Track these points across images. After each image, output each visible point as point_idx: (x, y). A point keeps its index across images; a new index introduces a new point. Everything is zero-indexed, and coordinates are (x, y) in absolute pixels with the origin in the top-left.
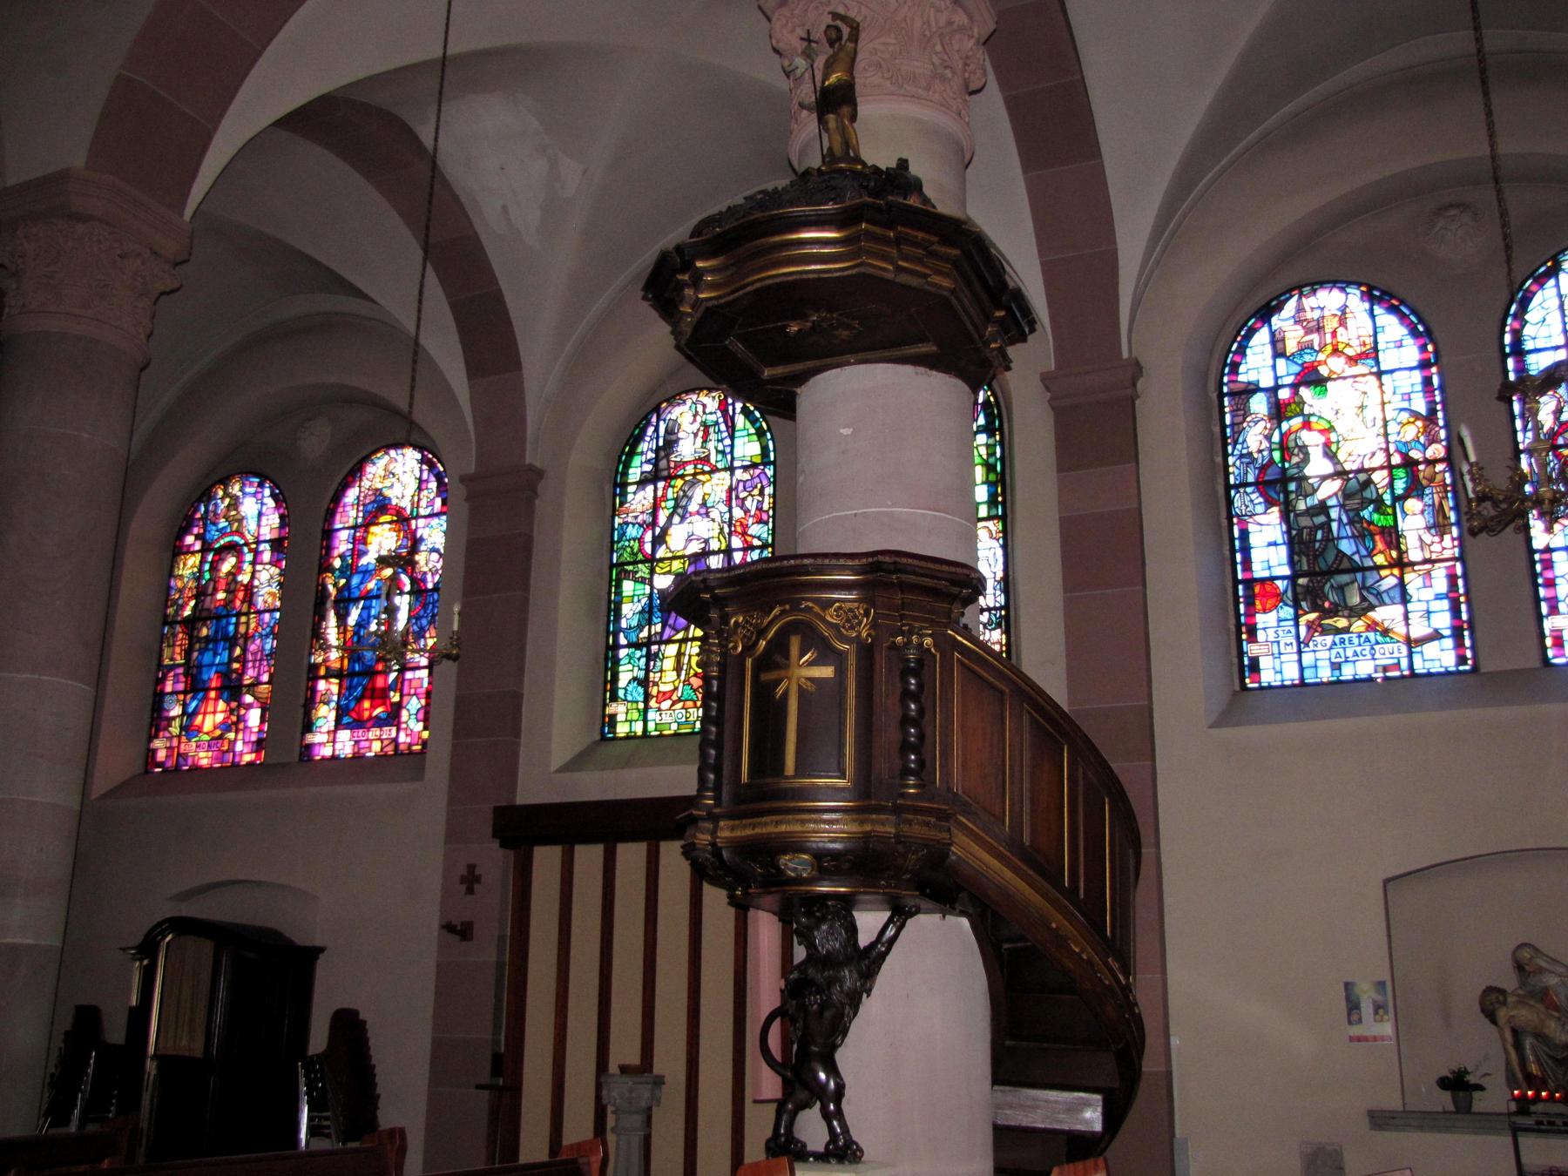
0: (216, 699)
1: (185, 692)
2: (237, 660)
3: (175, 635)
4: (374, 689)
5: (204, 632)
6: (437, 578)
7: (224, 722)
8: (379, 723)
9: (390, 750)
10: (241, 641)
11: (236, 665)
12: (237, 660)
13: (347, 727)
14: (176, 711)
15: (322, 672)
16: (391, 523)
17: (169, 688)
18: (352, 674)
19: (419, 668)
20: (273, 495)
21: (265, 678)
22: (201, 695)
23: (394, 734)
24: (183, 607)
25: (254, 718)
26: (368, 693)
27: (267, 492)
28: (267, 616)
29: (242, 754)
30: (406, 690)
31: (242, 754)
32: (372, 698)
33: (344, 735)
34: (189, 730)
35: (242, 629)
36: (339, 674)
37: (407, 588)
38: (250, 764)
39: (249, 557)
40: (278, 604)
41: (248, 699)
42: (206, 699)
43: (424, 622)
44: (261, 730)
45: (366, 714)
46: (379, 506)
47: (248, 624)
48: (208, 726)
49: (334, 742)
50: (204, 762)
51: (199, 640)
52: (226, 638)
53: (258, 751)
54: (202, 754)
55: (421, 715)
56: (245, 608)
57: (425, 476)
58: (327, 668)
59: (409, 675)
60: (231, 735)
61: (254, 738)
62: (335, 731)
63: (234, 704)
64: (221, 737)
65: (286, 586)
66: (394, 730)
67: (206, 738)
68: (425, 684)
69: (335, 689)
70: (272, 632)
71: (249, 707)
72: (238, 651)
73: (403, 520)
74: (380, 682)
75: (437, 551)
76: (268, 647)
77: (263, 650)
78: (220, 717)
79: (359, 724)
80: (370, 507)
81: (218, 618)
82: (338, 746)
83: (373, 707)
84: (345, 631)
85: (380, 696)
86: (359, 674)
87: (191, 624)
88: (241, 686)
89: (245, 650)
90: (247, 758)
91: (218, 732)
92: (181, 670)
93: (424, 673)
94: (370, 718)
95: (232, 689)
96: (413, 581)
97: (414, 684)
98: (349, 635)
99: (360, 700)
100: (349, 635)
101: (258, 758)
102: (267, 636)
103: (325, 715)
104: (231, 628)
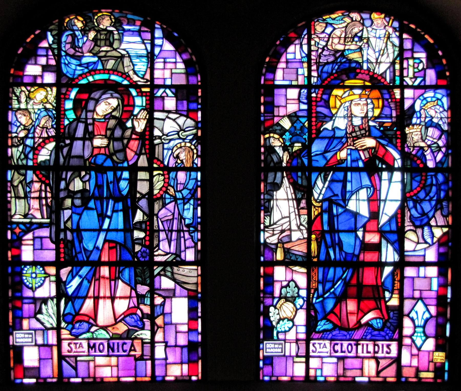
0: (114, 278)
1: (58, 264)
2: (139, 226)
3: (27, 184)
4: (360, 286)
5: (78, 185)
6: (439, 156)
7: (130, 312)
8: (374, 334)
9: (390, 374)
10: (143, 203)
11: (138, 234)
12: (139, 226)
13: (323, 335)
14: (48, 290)
15: (279, 256)
16: (363, 88)
17: (27, 254)
18: (328, 263)
19: (425, 264)
20: (167, 36)
21: (190, 255)
22: (84, 271)
23: (394, 353)
24: (36, 150)
25: (179, 309)
26: (353, 291)
27: (158, 33)
28: (182, 176)
29: (166, 362)
30: (407, 292)
31: (166, 362)
32: (359, 298)
33: (321, 347)
34: (74, 319)
35: (143, 188)
36: (307, 262)
37: (398, 164)
38: (178, 380)
39: (139, 101)
40: (198, 162)
41: (166, 283)
42: (94, 277)
43: (427, 207)
44: (191, 330)
45: (353, 319)
46: (342, 71)
47: (151, 181)
48: (105, 315)
49: (307, 357)
50: (106, 373)
51: (72, 195)
52: (117, 197)
53: (191, 362)
54: (100, 361)
55: (431, 329)
56: (143, 162)
57: (408, 45)
58: (287, 252)
59: (409, 272)
60: (146, 334)
61: (182, 340)
62: (308, 341)
63: (143, 289)
64: (128, 335)
65: (206, 139)
66: (394, 346)
67: (103, 334)
68: (435, 286)
69: (302, 281)
70: (193, 192)
71: (170, 295)
72: (139, 216)
73: (377, 85)
74: (369, 277)
75: (437, 126)
76: (188, 214)
77: (182, 218)
78: (122, 306)
79: (342, 330)
80: (328, 68)
81: (101, 170)
82: (314, 363)
83: (362, 312)
84: (309, 206)
85: (371, 296)
86: (336, 264)
87: (52, 173)
88: (152, 264)
89: (151, 214)
90: (175, 371)
91: (122, 328)
92: (45, 232)
93: (433, 271)
94: (359, 325)
95: (139, 266)
96: (405, 156)
97: (418, 284)
98: (315, 212)
99: (341, 299)
100: (315, 212)
101: (192, 371)
102: (185, 201)
103: (288, 317)
104: (124, 185)
